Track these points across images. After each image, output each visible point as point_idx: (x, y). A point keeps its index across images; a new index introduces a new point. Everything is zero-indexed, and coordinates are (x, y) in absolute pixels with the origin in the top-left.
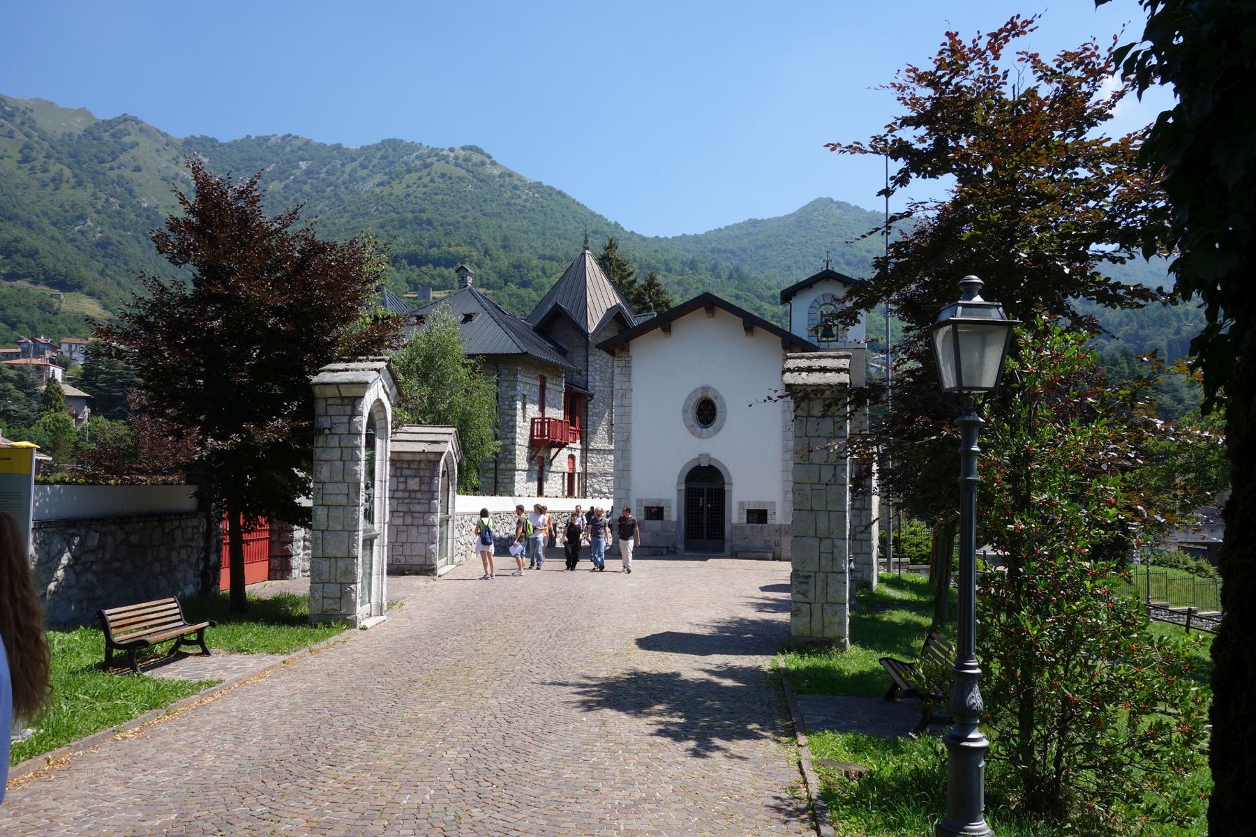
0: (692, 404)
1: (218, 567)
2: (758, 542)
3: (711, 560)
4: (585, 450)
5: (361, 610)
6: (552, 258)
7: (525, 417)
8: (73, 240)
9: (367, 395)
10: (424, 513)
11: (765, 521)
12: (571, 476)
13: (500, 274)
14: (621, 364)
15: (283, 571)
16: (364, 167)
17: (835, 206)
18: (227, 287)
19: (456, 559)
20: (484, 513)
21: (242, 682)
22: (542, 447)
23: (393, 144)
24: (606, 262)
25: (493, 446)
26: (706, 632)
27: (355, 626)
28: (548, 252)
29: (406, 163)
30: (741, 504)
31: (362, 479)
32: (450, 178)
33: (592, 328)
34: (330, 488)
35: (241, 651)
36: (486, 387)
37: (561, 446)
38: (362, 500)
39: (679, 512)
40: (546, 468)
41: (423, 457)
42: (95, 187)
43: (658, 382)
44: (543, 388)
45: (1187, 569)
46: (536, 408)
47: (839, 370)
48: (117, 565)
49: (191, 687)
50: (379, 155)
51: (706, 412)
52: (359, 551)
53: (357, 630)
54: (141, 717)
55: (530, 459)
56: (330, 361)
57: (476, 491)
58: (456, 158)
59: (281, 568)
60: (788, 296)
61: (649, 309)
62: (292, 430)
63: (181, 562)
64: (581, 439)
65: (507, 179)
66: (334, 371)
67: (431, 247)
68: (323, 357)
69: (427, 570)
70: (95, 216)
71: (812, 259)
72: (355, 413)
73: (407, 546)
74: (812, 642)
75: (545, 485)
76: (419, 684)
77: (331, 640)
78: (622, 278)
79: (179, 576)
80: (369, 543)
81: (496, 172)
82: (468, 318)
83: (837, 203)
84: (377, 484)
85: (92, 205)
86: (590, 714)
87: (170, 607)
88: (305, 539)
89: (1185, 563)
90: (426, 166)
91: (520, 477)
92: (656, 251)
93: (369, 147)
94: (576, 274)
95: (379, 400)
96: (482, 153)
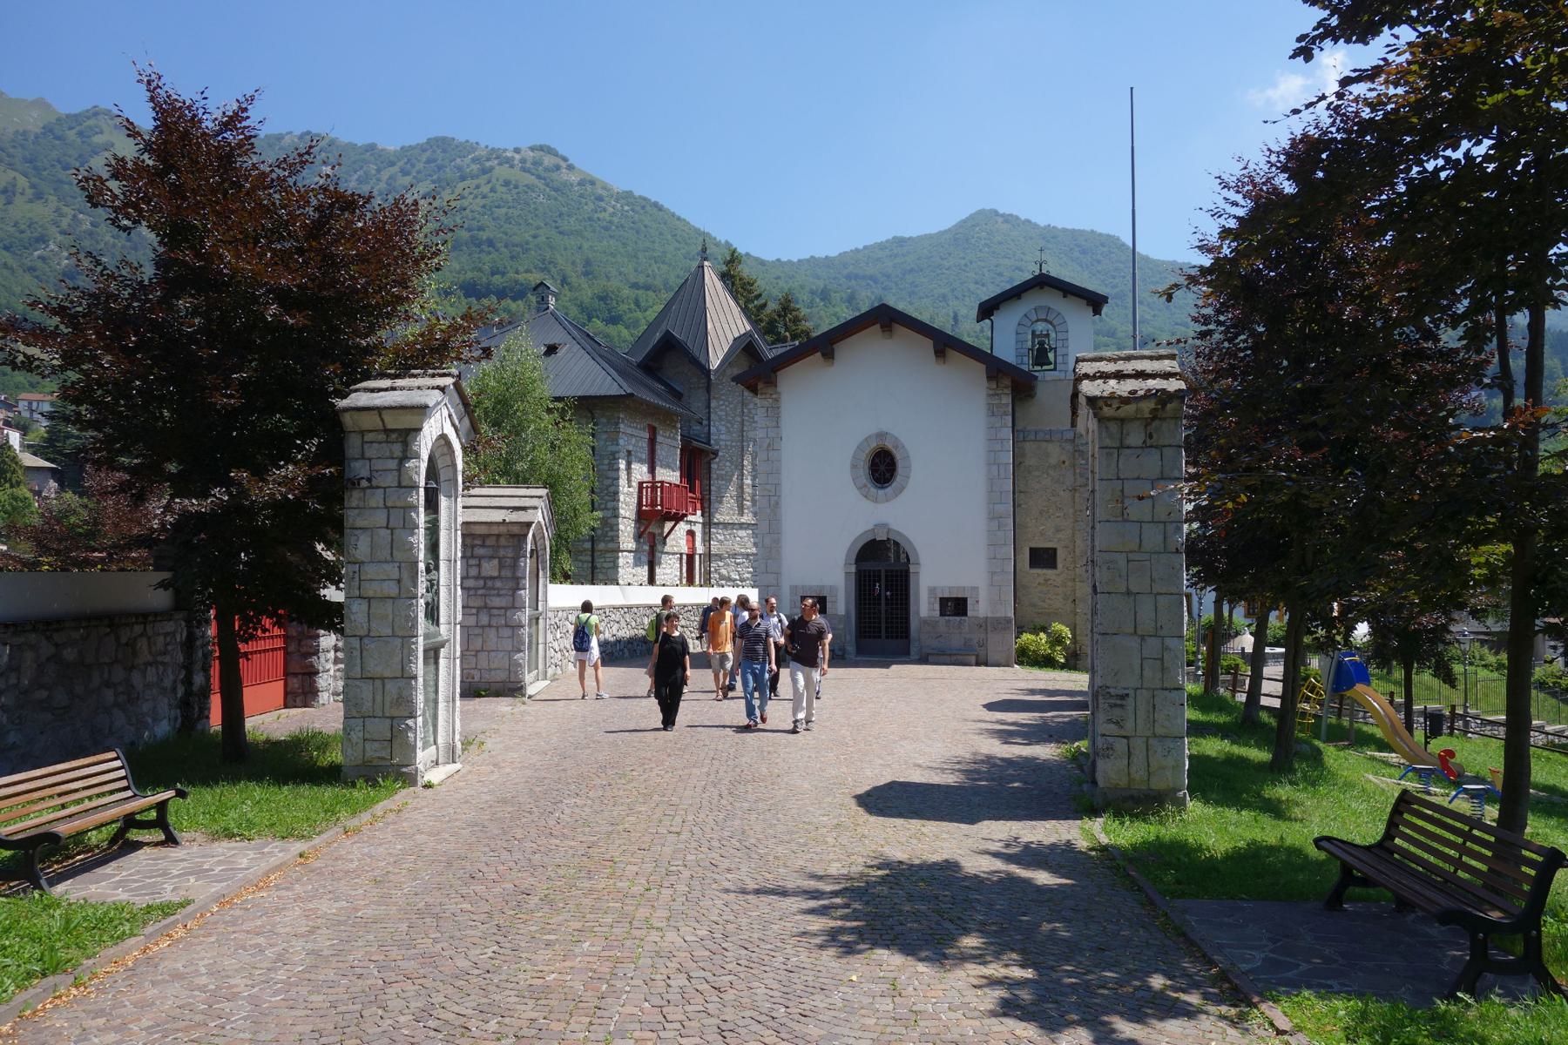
0: (863, 456)
1: (205, 693)
2: (956, 642)
3: (894, 667)
4: (708, 525)
5: (423, 756)
6: (647, 288)
7: (631, 479)
8: (32, 269)
9: (426, 427)
10: (506, 609)
11: (965, 613)
12: (691, 558)
13: (582, 308)
14: (766, 403)
15: (305, 694)
16: (405, 173)
17: (1000, 220)
18: (198, 255)
19: (550, 671)
20: (587, 607)
21: (223, 900)
22: (653, 520)
23: (443, 144)
24: (728, 278)
25: (589, 520)
26: (950, 779)
27: (413, 783)
28: (642, 280)
29: (459, 168)
30: (932, 590)
31: (421, 556)
32: (516, 187)
33: (715, 363)
34: (370, 571)
35: (230, 836)
36: (578, 439)
37: (678, 518)
38: (422, 589)
39: (847, 603)
40: (659, 547)
41: (503, 529)
42: (59, 200)
43: (818, 424)
44: (652, 442)
45: (1485, 666)
46: (645, 468)
47: (1167, 376)
48: (44, 694)
49: (132, 918)
50: (424, 158)
51: (882, 467)
52: (419, 667)
53: (419, 789)
54: (22, 996)
55: (638, 537)
56: (367, 376)
57: (567, 578)
58: (523, 161)
59: (301, 691)
60: (987, 310)
61: (784, 340)
62: (311, 481)
63: (148, 686)
64: (703, 509)
65: (589, 187)
66: (373, 390)
67: (493, 274)
68: (357, 370)
69: (513, 689)
70: (60, 238)
71: (972, 286)
72: (408, 454)
73: (483, 656)
74: (1132, 797)
75: (658, 570)
76: (534, 901)
77: (379, 809)
78: (748, 301)
79: (145, 707)
80: (433, 654)
81: (574, 178)
82: (551, 350)
83: (1003, 215)
84: (442, 565)
85: (56, 224)
86: (856, 961)
87: (110, 766)
88: (336, 649)
89: (1481, 659)
90: (484, 171)
91: (625, 560)
92: (778, 278)
93: (411, 148)
94: (692, 291)
95: (443, 437)
96: (556, 154)
